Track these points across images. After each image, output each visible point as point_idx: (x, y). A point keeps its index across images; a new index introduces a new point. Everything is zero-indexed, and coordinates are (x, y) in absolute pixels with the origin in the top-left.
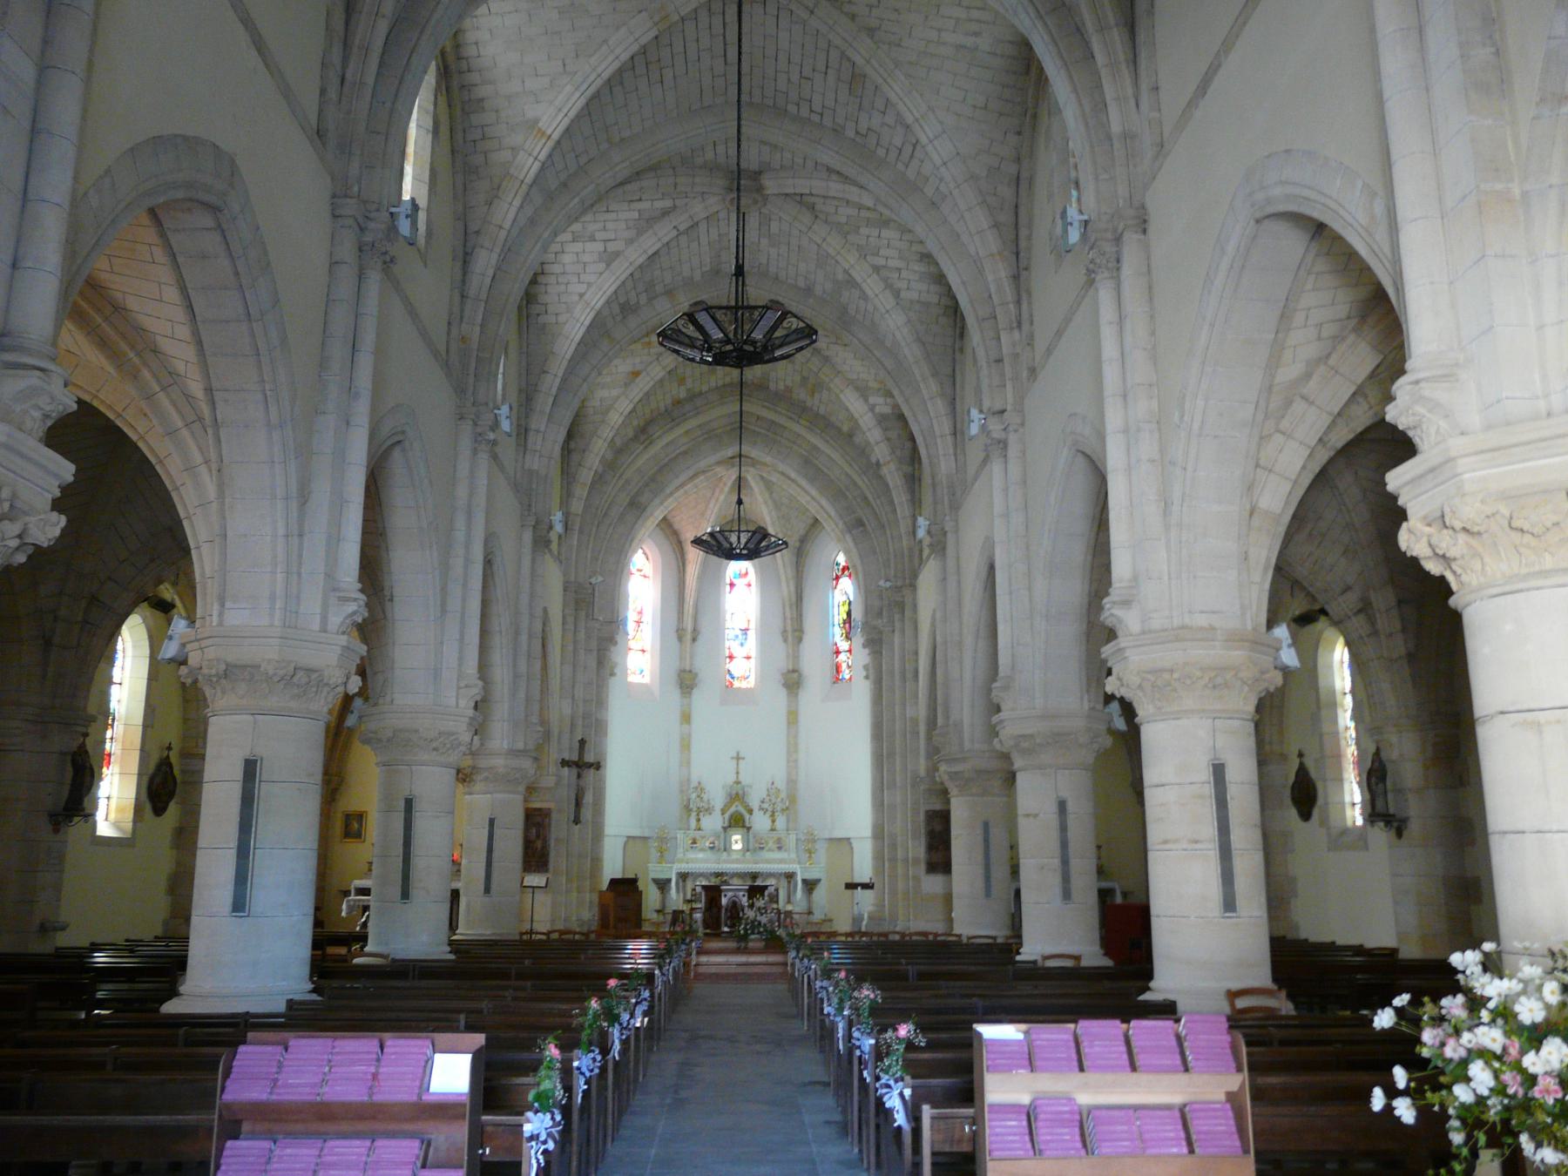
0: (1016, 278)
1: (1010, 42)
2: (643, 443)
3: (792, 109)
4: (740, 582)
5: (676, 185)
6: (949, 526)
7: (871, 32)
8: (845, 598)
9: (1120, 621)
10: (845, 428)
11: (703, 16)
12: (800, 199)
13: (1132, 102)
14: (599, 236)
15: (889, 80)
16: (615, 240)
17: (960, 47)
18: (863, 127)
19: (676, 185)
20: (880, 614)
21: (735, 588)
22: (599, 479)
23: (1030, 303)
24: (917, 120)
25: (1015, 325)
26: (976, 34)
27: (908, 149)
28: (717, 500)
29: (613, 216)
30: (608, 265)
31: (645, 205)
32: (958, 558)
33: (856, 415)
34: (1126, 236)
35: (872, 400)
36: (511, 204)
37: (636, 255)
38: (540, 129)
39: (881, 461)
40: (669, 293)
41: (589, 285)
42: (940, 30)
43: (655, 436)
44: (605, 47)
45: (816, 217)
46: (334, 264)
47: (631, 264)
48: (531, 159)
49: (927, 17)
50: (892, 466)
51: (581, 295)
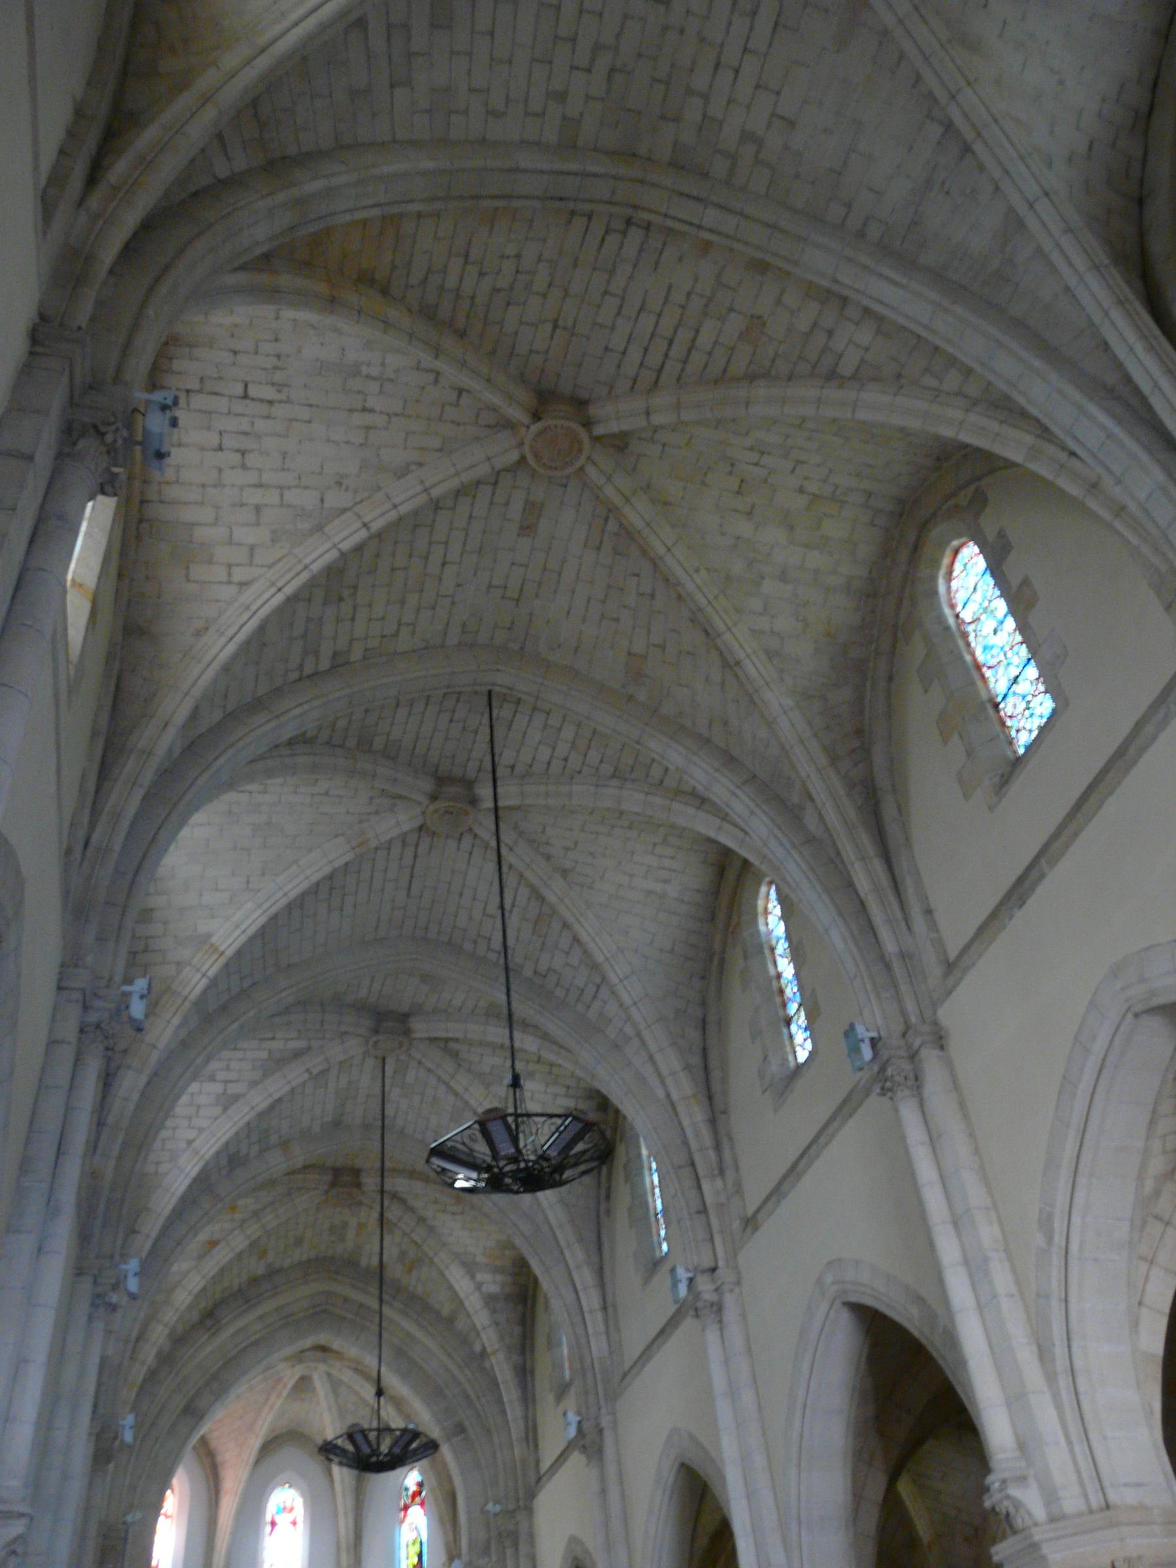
0: (713, 1122)
1: (698, 891)
2: (209, 1329)
3: (468, 946)
4: (283, 1520)
5: (322, 1023)
6: (605, 1421)
7: (565, 873)
8: (414, 1535)
9: (1018, 1505)
10: (446, 1311)
11: (396, 850)
12: (444, 1044)
13: (903, 924)
14: (221, 1076)
15: (581, 919)
16: (238, 1081)
17: (650, 893)
18: (543, 968)
19: (322, 1023)
20: (486, 1551)
21: (277, 1528)
22: (152, 1376)
23: (732, 1148)
24: (607, 959)
25: (716, 1172)
26: (665, 881)
27: (592, 989)
28: (271, 1408)
29: (239, 1054)
30: (225, 1109)
31: (277, 1045)
32: (619, 1463)
33: (462, 1295)
34: (924, 1053)
35: (479, 1277)
36: (169, 1022)
37: (259, 1100)
38: (212, 945)
39: (489, 1350)
40: (284, 1145)
41: (201, 1130)
42: (631, 876)
43: (224, 1321)
44: (295, 867)
45: (460, 1065)
46: (53, 1043)
47: (253, 1108)
48: (199, 976)
49: (620, 863)
50: (501, 1356)
51: (190, 1142)
